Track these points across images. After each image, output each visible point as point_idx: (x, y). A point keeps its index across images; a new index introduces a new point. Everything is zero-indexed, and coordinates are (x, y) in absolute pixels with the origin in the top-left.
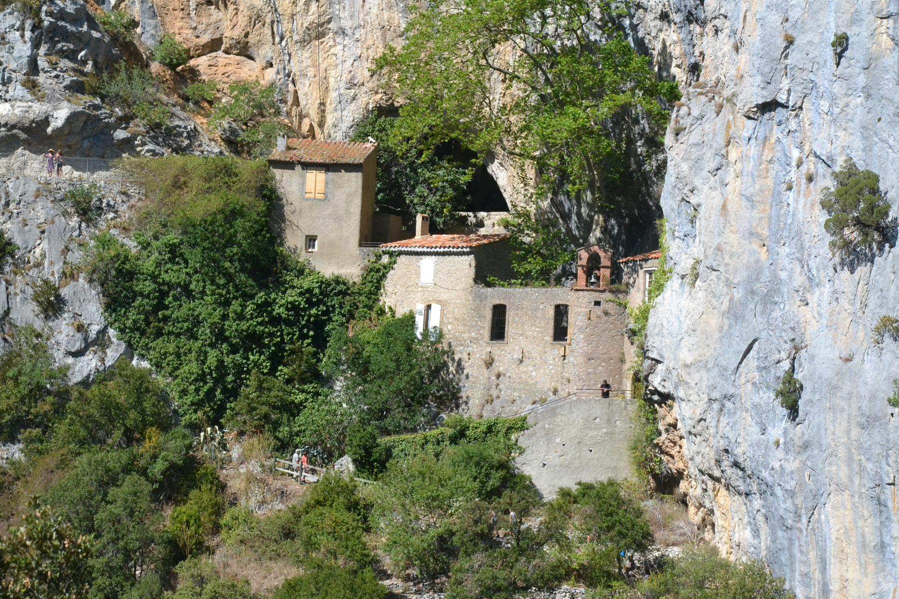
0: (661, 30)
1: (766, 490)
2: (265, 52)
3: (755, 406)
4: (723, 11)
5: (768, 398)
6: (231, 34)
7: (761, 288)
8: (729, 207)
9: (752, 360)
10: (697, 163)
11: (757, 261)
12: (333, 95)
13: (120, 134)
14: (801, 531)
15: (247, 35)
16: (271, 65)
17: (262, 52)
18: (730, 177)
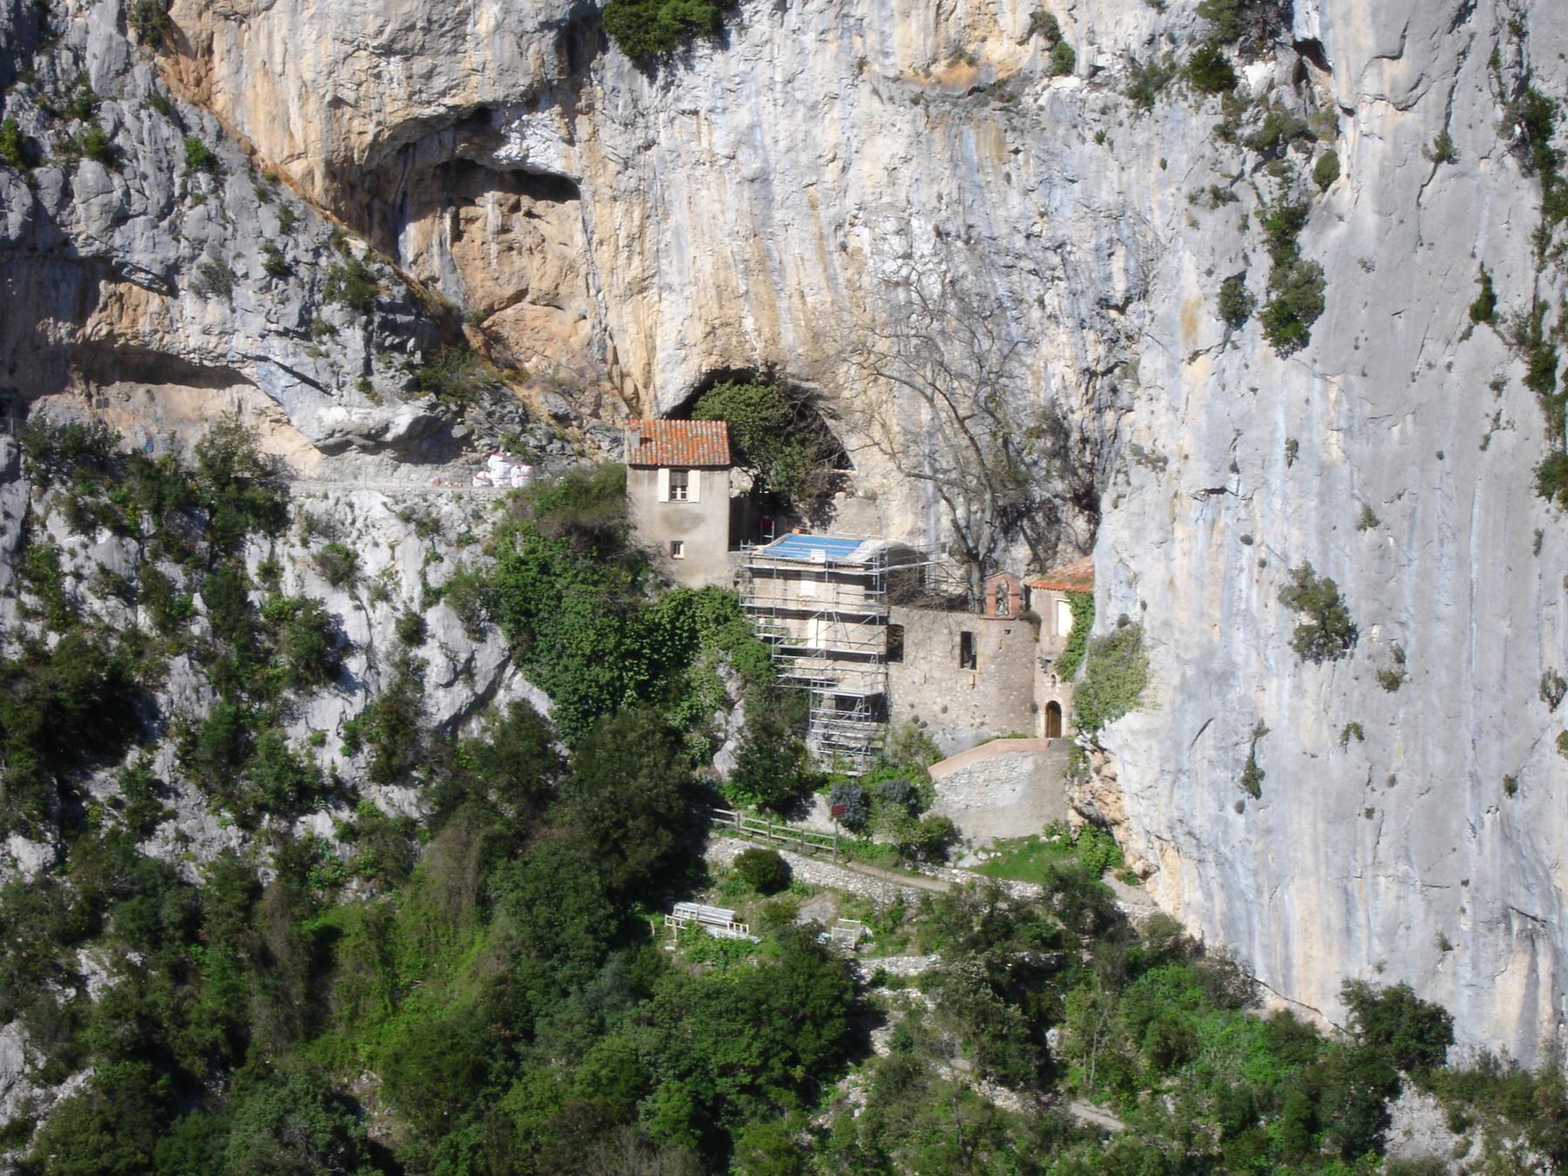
2: (578, 304)
3: (1213, 783)
4: (1159, 383)
6: (537, 285)
8: (1177, 583)
10: (1138, 534)
11: (1210, 642)
12: (660, 355)
13: (458, 432)
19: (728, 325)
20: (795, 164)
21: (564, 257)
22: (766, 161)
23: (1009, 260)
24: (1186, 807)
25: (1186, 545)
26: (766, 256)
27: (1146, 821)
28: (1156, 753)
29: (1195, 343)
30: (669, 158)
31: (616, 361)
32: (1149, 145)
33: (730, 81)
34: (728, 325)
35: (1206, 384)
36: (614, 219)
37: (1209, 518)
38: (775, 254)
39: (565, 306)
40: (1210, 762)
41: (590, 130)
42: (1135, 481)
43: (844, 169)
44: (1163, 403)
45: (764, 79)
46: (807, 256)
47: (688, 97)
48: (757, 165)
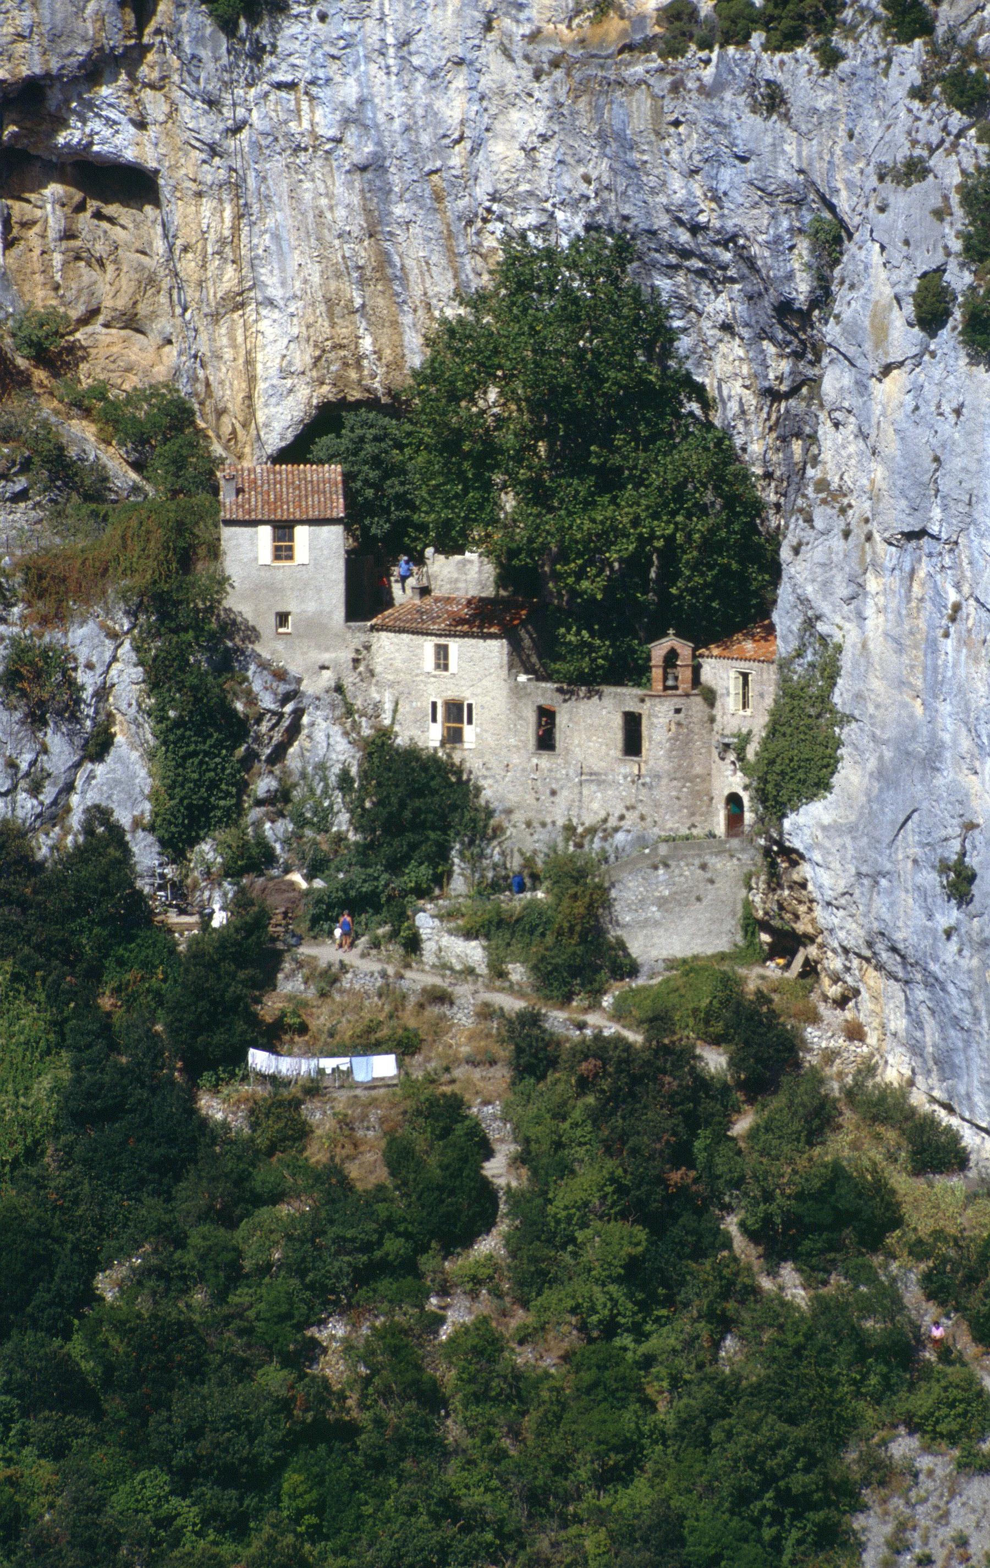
0: (721, 341)
1: (933, 983)
2: (163, 325)
5: (931, 879)
7: (919, 748)
8: (871, 646)
9: (910, 835)
10: (826, 586)
11: (912, 716)
12: (261, 385)
14: (981, 1035)
15: (135, 303)
16: (170, 342)
17: (157, 326)
18: (869, 611)
19: (342, 347)
20: (415, 146)
21: (141, 268)
22: (379, 143)
23: (673, 258)
24: (887, 917)
25: (881, 600)
26: (384, 259)
27: (842, 934)
28: (850, 852)
29: (886, 354)
30: (263, 143)
31: (209, 394)
32: (833, 110)
33: (333, 44)
34: (342, 347)
35: (902, 405)
36: (213, 217)
37: (907, 567)
38: (396, 259)
39: (146, 329)
40: (915, 861)
41: (166, 108)
42: (819, 524)
43: (473, 151)
44: (852, 428)
45: (374, 41)
46: (434, 259)
47: (284, 66)
48: (369, 148)
